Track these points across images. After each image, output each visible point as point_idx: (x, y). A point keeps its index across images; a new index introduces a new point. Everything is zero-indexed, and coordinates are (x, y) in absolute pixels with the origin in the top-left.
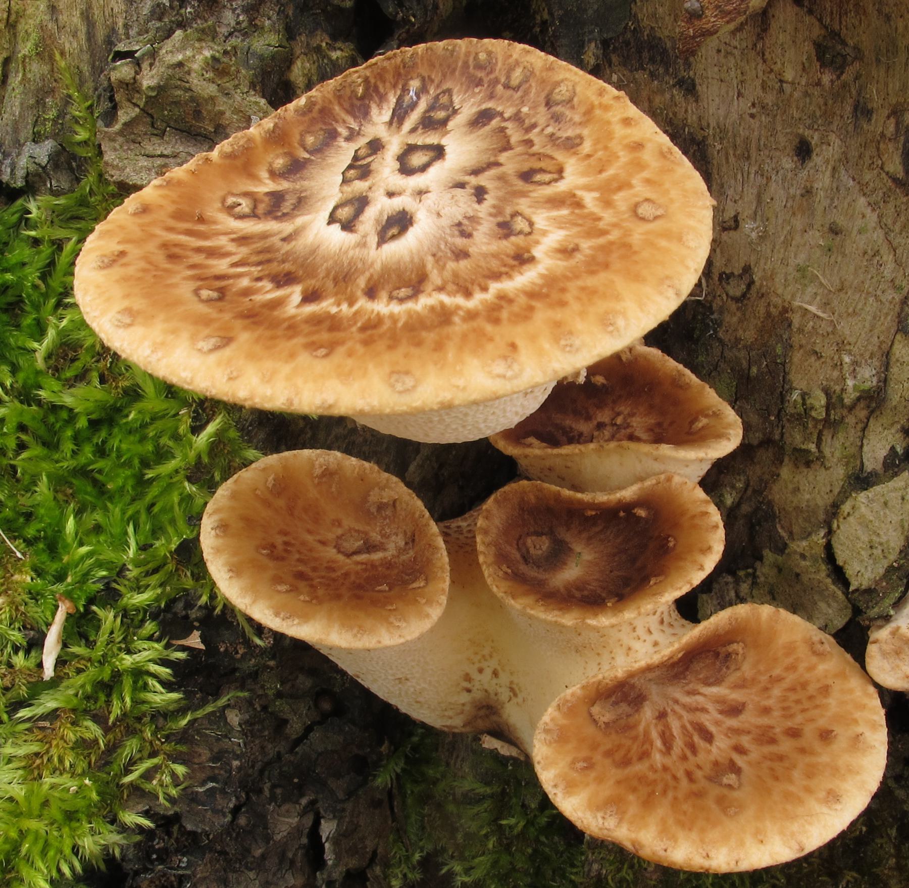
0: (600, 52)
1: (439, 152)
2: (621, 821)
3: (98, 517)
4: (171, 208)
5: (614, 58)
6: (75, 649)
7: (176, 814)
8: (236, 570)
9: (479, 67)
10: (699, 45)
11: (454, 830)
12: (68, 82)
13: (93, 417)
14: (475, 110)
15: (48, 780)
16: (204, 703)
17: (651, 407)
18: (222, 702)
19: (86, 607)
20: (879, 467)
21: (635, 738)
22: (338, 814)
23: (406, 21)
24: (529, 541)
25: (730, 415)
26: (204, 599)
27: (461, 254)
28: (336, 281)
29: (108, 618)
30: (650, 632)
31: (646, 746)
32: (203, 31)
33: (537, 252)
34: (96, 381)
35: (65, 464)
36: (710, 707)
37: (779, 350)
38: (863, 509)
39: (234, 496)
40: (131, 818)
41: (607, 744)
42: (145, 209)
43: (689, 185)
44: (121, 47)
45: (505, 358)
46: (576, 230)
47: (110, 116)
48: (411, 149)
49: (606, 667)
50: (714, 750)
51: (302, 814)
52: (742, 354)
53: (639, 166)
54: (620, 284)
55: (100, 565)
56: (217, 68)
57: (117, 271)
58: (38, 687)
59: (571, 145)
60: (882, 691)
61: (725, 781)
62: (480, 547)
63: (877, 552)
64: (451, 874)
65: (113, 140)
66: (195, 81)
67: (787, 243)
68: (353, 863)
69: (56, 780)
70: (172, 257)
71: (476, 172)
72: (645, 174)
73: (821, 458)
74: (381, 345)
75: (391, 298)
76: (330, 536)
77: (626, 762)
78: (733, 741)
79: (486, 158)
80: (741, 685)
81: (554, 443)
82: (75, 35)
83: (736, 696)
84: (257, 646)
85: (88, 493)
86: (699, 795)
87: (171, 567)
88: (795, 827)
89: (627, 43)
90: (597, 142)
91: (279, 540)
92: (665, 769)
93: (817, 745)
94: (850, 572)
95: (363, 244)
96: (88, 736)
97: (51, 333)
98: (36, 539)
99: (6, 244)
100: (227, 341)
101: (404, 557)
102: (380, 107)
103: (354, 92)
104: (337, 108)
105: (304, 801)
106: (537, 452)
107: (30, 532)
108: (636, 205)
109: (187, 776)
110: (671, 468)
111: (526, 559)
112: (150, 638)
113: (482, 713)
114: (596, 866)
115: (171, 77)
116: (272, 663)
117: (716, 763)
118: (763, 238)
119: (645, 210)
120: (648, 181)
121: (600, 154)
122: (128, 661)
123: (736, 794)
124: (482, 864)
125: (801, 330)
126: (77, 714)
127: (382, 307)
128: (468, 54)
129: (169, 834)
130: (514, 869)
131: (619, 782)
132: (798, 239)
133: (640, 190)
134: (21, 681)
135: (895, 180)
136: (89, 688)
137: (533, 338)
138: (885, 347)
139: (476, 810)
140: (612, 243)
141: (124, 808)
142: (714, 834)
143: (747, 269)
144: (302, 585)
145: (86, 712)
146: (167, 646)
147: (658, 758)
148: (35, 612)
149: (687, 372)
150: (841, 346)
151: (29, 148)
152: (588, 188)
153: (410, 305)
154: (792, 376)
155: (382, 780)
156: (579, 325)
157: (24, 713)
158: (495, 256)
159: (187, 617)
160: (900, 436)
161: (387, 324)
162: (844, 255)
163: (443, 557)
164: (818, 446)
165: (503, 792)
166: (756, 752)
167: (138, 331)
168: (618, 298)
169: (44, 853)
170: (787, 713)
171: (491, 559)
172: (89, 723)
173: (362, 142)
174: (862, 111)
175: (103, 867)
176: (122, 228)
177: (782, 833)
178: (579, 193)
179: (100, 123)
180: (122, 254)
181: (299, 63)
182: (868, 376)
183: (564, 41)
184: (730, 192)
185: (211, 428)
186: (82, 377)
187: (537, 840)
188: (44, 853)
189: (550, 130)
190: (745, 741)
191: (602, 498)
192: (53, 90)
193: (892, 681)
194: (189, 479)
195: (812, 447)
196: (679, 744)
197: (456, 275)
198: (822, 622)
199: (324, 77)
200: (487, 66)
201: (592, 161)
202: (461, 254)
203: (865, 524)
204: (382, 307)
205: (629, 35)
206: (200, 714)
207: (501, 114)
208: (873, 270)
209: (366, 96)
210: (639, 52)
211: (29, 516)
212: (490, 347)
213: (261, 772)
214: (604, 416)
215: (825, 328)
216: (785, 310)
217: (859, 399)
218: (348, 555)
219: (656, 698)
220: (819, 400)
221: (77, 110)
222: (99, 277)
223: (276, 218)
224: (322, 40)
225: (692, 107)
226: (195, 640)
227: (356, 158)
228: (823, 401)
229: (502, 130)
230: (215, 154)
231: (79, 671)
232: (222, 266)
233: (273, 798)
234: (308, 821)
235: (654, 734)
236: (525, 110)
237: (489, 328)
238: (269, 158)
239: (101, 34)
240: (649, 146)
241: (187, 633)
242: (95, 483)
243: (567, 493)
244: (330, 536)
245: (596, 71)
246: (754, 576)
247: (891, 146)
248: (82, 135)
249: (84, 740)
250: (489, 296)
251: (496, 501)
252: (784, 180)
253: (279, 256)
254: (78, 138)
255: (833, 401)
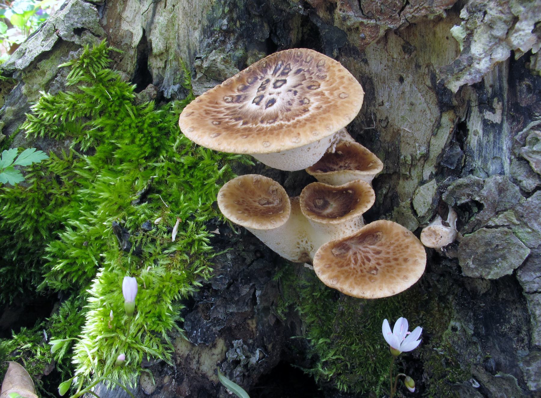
0: (338, 52)
1: (285, 81)
2: (338, 282)
3: (190, 195)
4: (209, 100)
5: (343, 54)
6: (181, 233)
7: (210, 284)
8: (226, 207)
9: (298, 56)
10: (365, 48)
11: (299, 297)
12: (183, 67)
13: (190, 165)
14: (296, 69)
15: (172, 271)
16: (220, 251)
17: (356, 161)
18: (226, 251)
19: (185, 221)
20: (428, 179)
21: (346, 260)
22: (261, 289)
23: (281, 45)
24: (317, 201)
25: (380, 162)
26: (220, 219)
27: (288, 110)
28: (253, 119)
29: (191, 224)
30: (351, 227)
31: (349, 262)
32: (220, 50)
33: (310, 109)
34: (190, 155)
35: (181, 180)
36: (371, 251)
37: (397, 143)
38: (422, 191)
39: (228, 187)
40: (196, 283)
41: (336, 261)
42: (201, 101)
43: (357, 88)
44: (198, 56)
45: (296, 137)
46: (322, 102)
47: (195, 76)
48: (277, 81)
49: (337, 237)
50: (370, 264)
51: (250, 289)
52: (387, 145)
53: (342, 83)
54: (332, 116)
55: (190, 209)
56: (225, 61)
57: (191, 117)
58: (171, 244)
59: (323, 78)
60: (427, 249)
61: (372, 272)
62: (301, 202)
63: (426, 205)
64: (298, 311)
65: (195, 83)
66: (218, 65)
67: (398, 109)
68: (266, 304)
69: (175, 271)
70: (207, 113)
71: (295, 87)
72: (344, 85)
73: (410, 176)
74: (262, 135)
75: (267, 123)
76: (257, 200)
77: (342, 266)
78: (377, 262)
79: (298, 83)
80: (381, 245)
81: (325, 171)
82: (185, 53)
83: (379, 248)
84: (236, 234)
85: (188, 188)
86: (364, 276)
87: (211, 209)
88: (392, 286)
89: (346, 49)
90: (331, 77)
91: (241, 200)
92: (354, 269)
93: (403, 263)
94: (418, 211)
95: (261, 108)
96: (184, 258)
97: (178, 141)
98: (172, 202)
99: (166, 115)
100: (219, 134)
101: (279, 206)
102: (270, 70)
103: (263, 66)
104: (258, 71)
105: (251, 284)
106: (320, 174)
107: (170, 200)
108: (340, 94)
109: (213, 272)
110: (359, 178)
111: (316, 206)
112: (204, 230)
113: (304, 255)
114: (341, 308)
115: (212, 64)
116: (241, 240)
117: (371, 268)
118: (391, 107)
119: (342, 95)
120: (344, 87)
121: (331, 80)
122: (197, 237)
123: (375, 276)
124: (307, 307)
125: (403, 136)
126: (181, 252)
127: (265, 125)
128: (295, 53)
129: (209, 291)
130: (317, 310)
131: (339, 272)
132: (401, 108)
133: (341, 89)
134: (165, 242)
135: (429, 87)
136: (185, 245)
137: (305, 132)
138: (428, 140)
139: (306, 290)
140: (331, 105)
141: (195, 280)
142: (366, 287)
143: (387, 118)
144: (246, 212)
145: (184, 252)
146: (209, 233)
147: (352, 266)
148: (170, 222)
149: (367, 150)
150: (416, 140)
151: (172, 87)
152: (326, 90)
153: (272, 124)
154: (401, 151)
155: (276, 278)
156: (319, 128)
157: (166, 251)
158: (298, 110)
159: (215, 224)
160: (434, 168)
161: (265, 129)
162: (415, 112)
163: (289, 204)
164: (410, 172)
165: (314, 285)
166: (383, 265)
167: (195, 132)
168: (331, 120)
169: (170, 292)
170: (395, 254)
171: (304, 205)
172: (185, 255)
173: (265, 80)
174: (418, 66)
175: (187, 298)
176: (194, 106)
177: (388, 287)
178: (324, 91)
179: (192, 78)
180: (193, 112)
181: (249, 59)
182: (423, 150)
183: (327, 49)
184: (380, 94)
185: (223, 168)
186: (186, 154)
187: (324, 300)
188: (170, 292)
189: (317, 74)
190: (380, 262)
191: (337, 187)
192: (179, 70)
193: (429, 244)
194: (216, 183)
195: (408, 173)
196: (360, 262)
197: (286, 116)
198: (411, 228)
199: (256, 61)
200: (300, 56)
201: (329, 82)
202: (288, 110)
203: (422, 196)
204: (265, 125)
205: (346, 46)
206: (218, 254)
207: (304, 70)
208: (424, 116)
209: (266, 67)
210: (350, 51)
211: (170, 195)
212: (292, 134)
213: (238, 274)
214: (342, 164)
215: (410, 135)
216: (398, 130)
217: (421, 157)
218: (262, 205)
219: (354, 248)
220: (409, 158)
221: (186, 75)
222: (186, 119)
223: (238, 102)
224: (256, 52)
225: (367, 67)
226: (217, 231)
227: (262, 85)
228: (410, 158)
229: (304, 74)
230: (222, 85)
231: (182, 239)
232: (221, 116)
233: (241, 282)
234: (252, 291)
235: (352, 259)
236: (311, 68)
237: (293, 129)
238: (238, 86)
239: (192, 52)
240: (346, 77)
241: (215, 229)
242: (190, 185)
243: (327, 185)
244: (257, 200)
245: (337, 59)
246: (391, 215)
247: (427, 77)
248: (187, 82)
249: (183, 260)
250: (294, 121)
251: (306, 188)
252: (396, 89)
253: (238, 113)
254: (186, 83)
255: (413, 158)
